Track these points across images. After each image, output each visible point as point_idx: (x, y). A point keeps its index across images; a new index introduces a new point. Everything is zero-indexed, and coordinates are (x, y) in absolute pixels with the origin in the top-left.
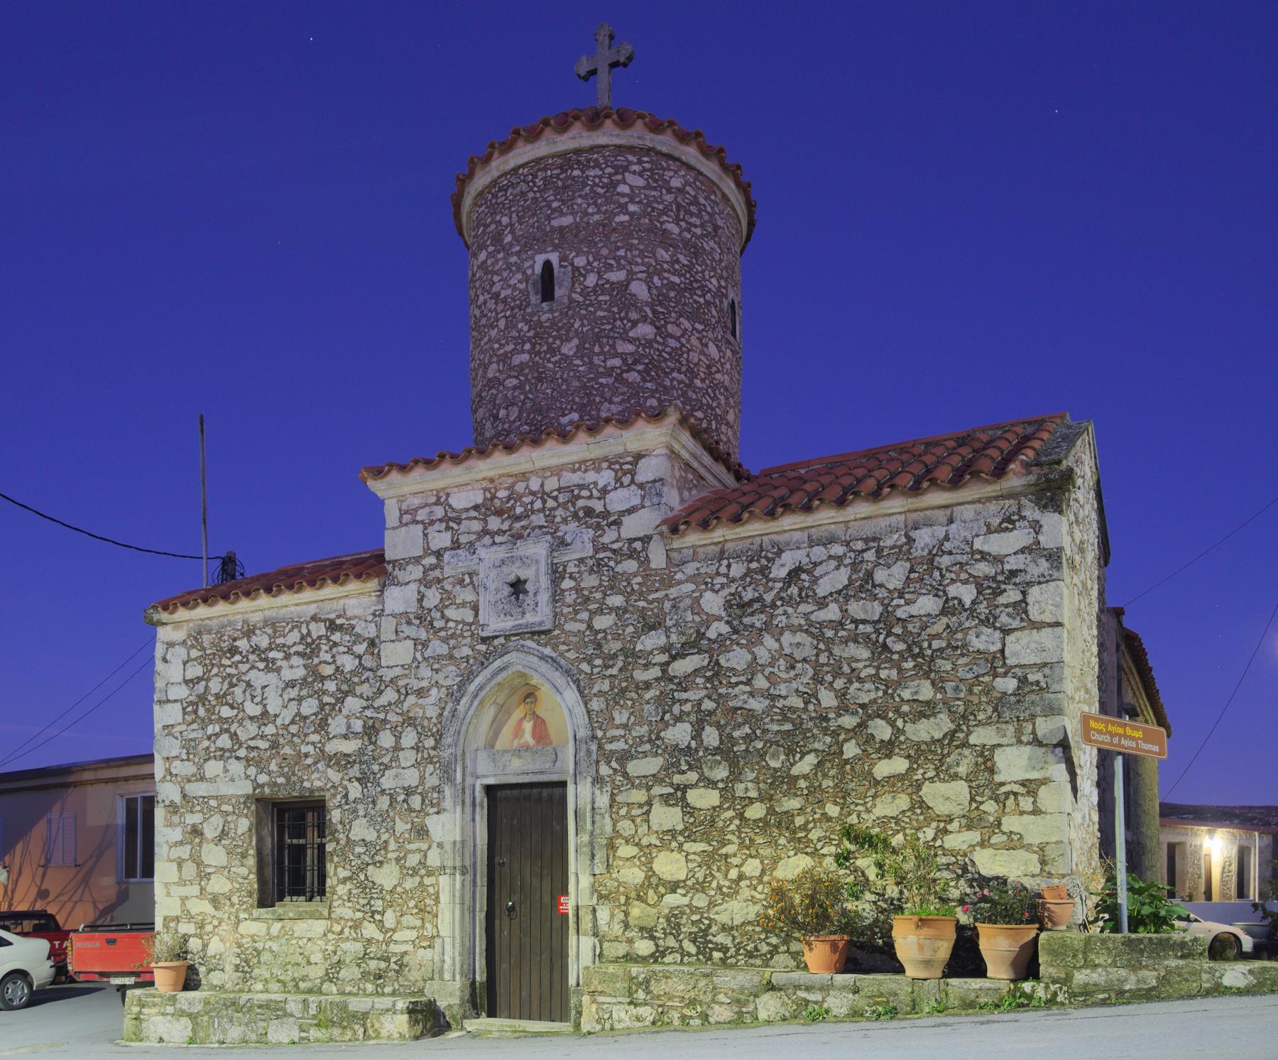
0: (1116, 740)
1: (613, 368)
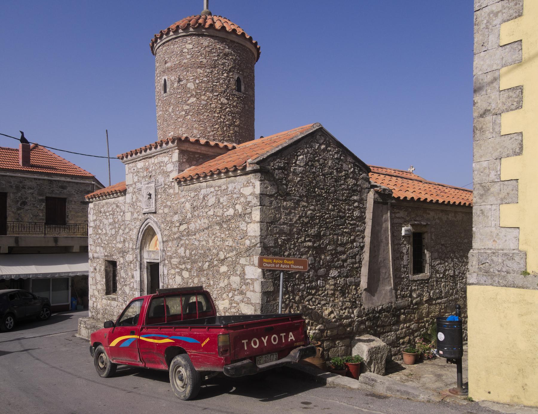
0: (278, 266)
1: (182, 116)
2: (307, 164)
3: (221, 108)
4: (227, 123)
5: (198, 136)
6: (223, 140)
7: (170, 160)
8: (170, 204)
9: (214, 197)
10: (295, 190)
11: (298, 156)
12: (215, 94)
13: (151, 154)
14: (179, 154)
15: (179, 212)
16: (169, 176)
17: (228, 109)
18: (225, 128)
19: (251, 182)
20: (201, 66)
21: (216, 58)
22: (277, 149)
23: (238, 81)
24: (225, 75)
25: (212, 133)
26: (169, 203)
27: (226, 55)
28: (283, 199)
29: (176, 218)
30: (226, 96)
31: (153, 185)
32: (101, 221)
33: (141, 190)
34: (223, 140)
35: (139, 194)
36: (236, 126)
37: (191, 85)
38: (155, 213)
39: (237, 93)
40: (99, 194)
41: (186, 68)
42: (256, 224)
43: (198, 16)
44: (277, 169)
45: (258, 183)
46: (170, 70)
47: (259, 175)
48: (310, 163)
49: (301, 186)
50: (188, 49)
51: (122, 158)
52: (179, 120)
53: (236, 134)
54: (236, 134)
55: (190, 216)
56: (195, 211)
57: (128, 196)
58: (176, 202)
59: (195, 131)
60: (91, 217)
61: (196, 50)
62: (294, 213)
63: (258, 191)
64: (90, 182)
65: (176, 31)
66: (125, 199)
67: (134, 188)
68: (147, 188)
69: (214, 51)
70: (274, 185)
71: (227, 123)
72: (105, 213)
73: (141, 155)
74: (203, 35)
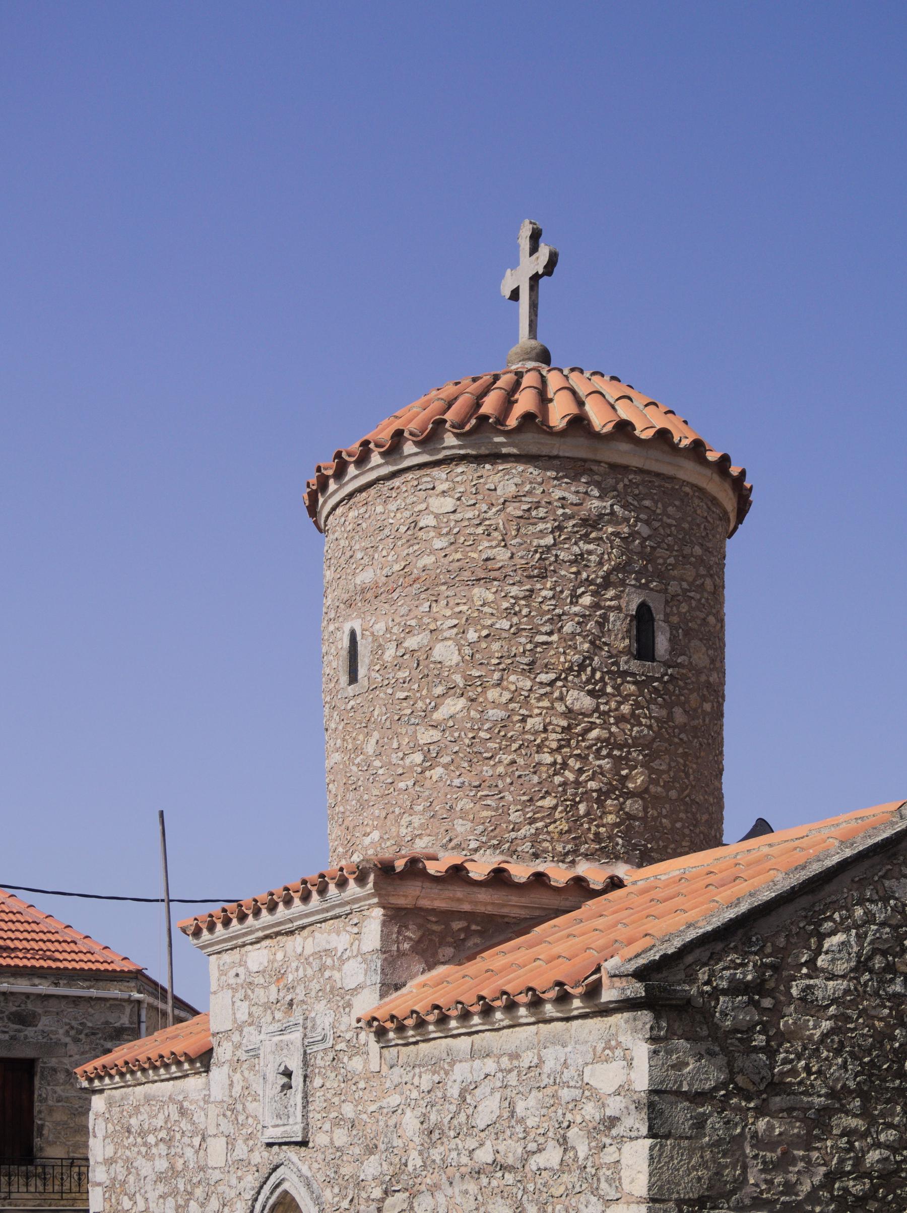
1: (411, 768)
2: (862, 965)
3: (567, 729)
4: (592, 785)
5: (473, 845)
6: (575, 852)
7: (355, 947)
8: (351, 1115)
9: (498, 1095)
10: (807, 1069)
11: (822, 937)
12: (544, 678)
13: (291, 921)
14: (384, 924)
15: (382, 1147)
16: (349, 1005)
17: (594, 733)
18: (582, 808)
19: (619, 1043)
20: (489, 574)
21: (549, 540)
22: (731, 914)
23: (643, 619)
24: (587, 600)
25: (527, 830)
26: (348, 1110)
27: (591, 523)
28: (755, 1109)
29: (372, 1167)
30: (588, 681)
31: (296, 1036)
32: (129, 1164)
33: (257, 1056)
34: (575, 852)
35: (252, 1068)
36: (631, 794)
37: (447, 653)
38: (304, 1143)
39: (635, 666)
40: (120, 1062)
41: (429, 587)
42: (634, 1207)
43: (487, 379)
44: (724, 992)
45: (641, 1050)
46: (369, 595)
47: (646, 1017)
48: (878, 962)
49: (838, 1052)
50: (437, 516)
51: (197, 933)
52: (402, 785)
53: (629, 828)
54: (629, 828)
55: (419, 1163)
56: (434, 1145)
57: (218, 1074)
58: (373, 1108)
59: (461, 827)
60: (98, 1149)
61: (470, 515)
62: (808, 1160)
63: (641, 1082)
64: (125, 996)
65: (393, 449)
66: (208, 1084)
67: (238, 1046)
68: (279, 1047)
69: (542, 512)
70: (711, 1054)
71: (592, 785)
72: (143, 1134)
73: (257, 924)
74: (495, 457)
